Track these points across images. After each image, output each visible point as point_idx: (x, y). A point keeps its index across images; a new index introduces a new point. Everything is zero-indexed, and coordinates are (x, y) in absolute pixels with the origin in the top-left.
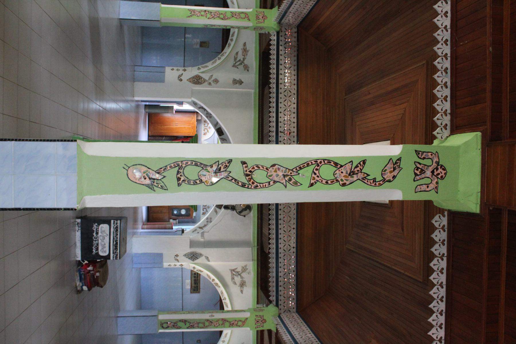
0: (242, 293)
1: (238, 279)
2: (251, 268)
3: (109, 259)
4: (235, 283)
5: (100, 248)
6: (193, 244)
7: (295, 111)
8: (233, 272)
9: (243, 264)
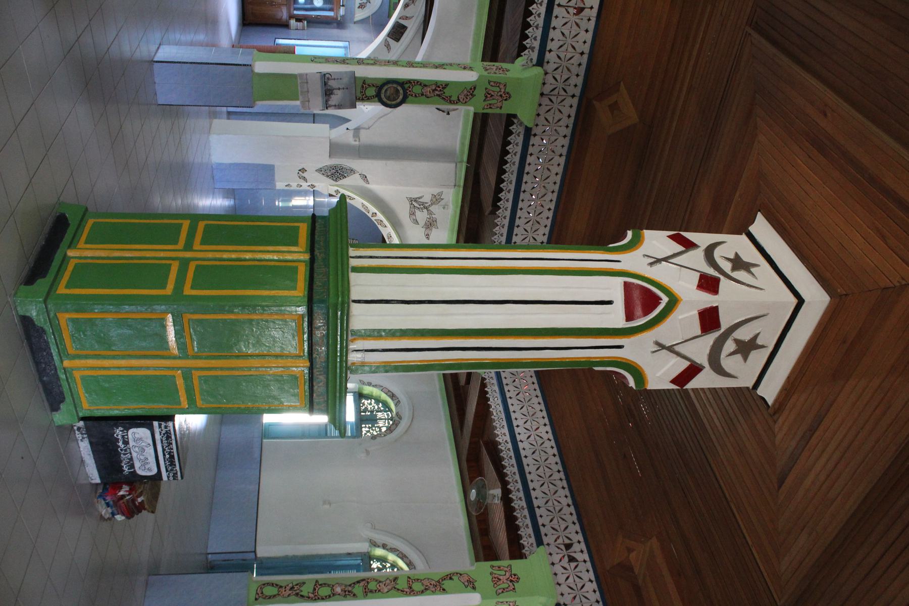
1: (422, 216)
3: (161, 478)
5: (137, 465)
6: (335, 149)
9: (436, 191)
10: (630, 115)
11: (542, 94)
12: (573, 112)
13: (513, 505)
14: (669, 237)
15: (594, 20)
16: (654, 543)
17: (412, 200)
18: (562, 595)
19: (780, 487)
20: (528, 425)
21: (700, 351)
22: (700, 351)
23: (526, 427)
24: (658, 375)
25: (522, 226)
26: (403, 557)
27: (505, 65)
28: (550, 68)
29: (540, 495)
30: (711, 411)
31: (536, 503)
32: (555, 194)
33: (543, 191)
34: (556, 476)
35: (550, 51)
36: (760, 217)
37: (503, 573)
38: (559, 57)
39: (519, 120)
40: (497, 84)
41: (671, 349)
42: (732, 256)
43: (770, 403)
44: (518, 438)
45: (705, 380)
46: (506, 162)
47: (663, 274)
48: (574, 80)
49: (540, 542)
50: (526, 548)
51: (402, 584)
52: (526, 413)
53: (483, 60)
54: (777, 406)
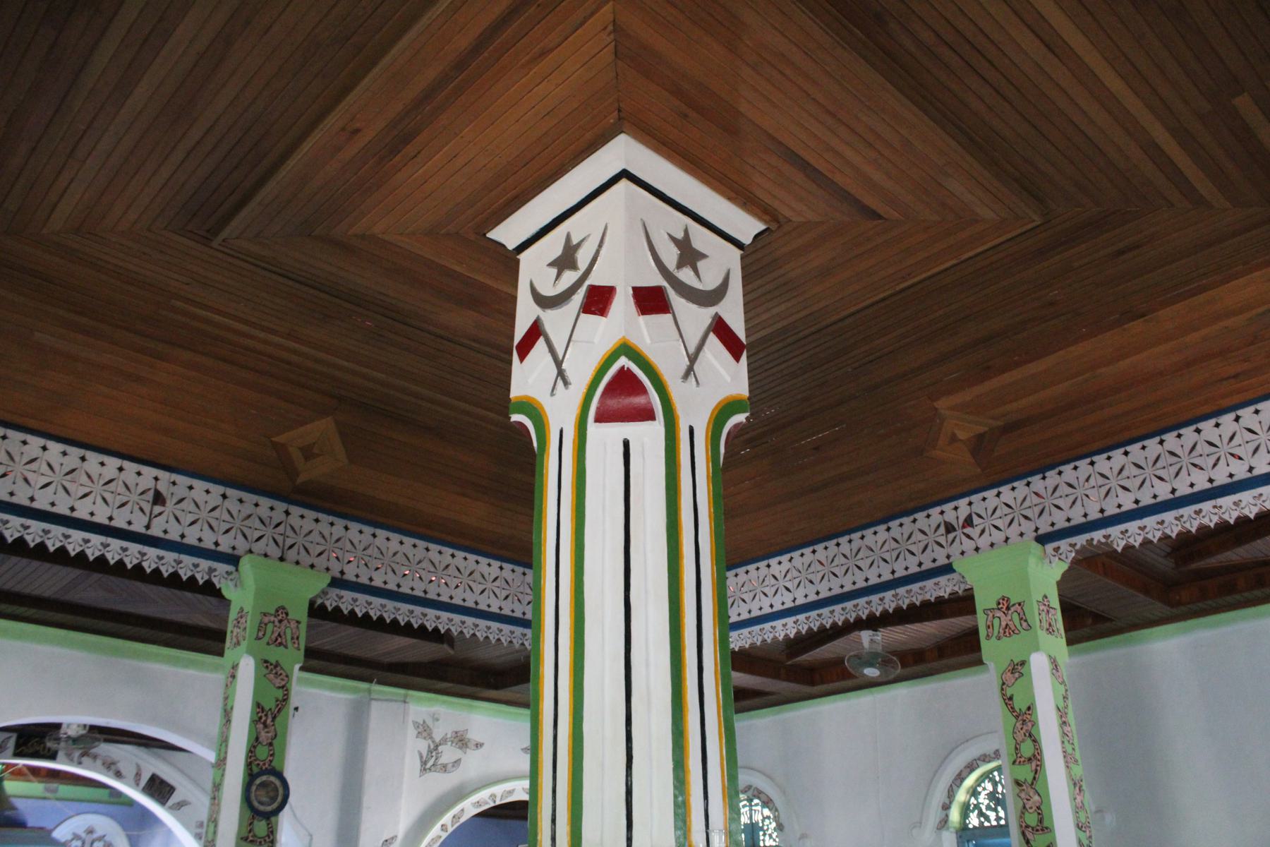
0: (482, 745)
1: (449, 754)
2: (424, 709)
4: (457, 763)
7: (75, 452)
8: (428, 765)
9: (411, 732)
10: (322, 429)
11: (282, 559)
12: (311, 514)
13: (878, 614)
14: (522, 358)
15: (174, 477)
16: (943, 404)
17: (424, 769)
18: (1022, 535)
19: (880, 217)
20: (770, 591)
21: (695, 318)
22: (695, 318)
23: (783, 590)
24: (728, 379)
25: (476, 597)
26: (960, 778)
27: (233, 614)
28: (242, 545)
29: (849, 577)
30: (764, 317)
31: (887, 576)
32: (431, 546)
33: (425, 564)
34: (845, 548)
35: (217, 544)
36: (495, 234)
37: (996, 622)
38: (227, 531)
39: (316, 597)
40: (262, 626)
41: (693, 359)
42: (554, 271)
43: (761, 227)
44: (789, 604)
45: (733, 312)
46: (381, 618)
47: (581, 367)
48: (263, 511)
49: (947, 569)
50: (956, 589)
51: (1025, 773)
52: (752, 595)
53: (220, 653)
54: (767, 217)
